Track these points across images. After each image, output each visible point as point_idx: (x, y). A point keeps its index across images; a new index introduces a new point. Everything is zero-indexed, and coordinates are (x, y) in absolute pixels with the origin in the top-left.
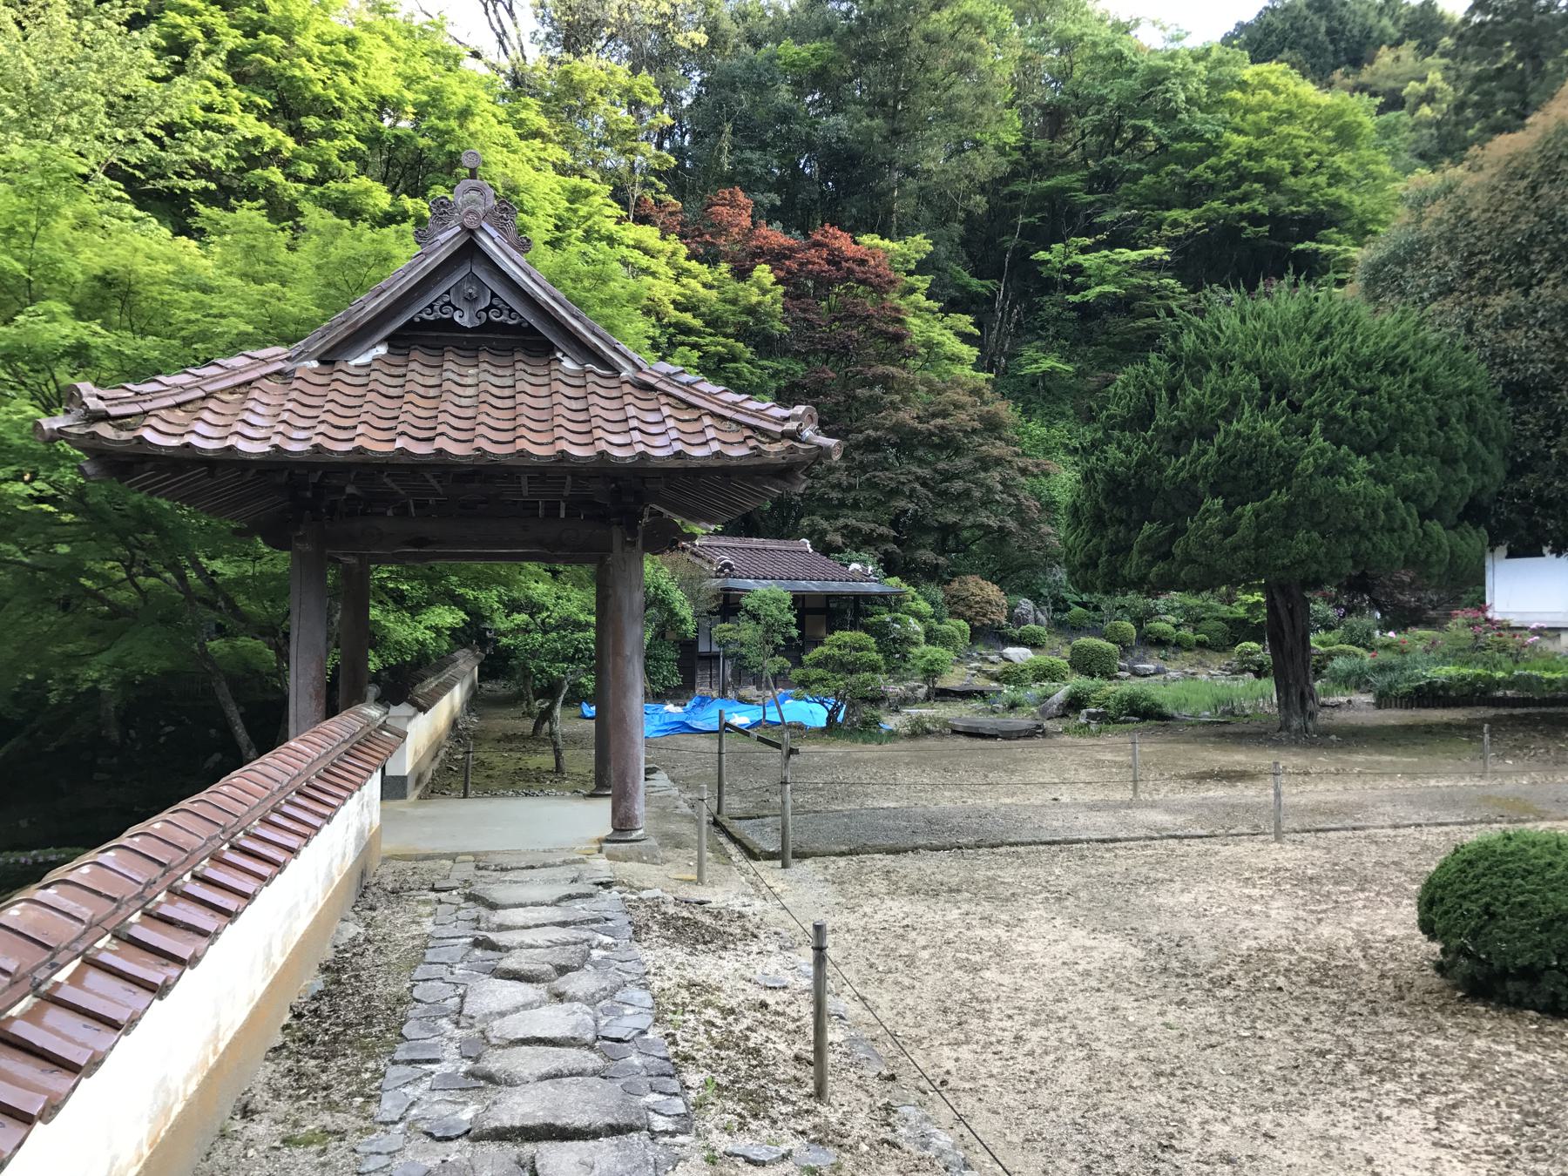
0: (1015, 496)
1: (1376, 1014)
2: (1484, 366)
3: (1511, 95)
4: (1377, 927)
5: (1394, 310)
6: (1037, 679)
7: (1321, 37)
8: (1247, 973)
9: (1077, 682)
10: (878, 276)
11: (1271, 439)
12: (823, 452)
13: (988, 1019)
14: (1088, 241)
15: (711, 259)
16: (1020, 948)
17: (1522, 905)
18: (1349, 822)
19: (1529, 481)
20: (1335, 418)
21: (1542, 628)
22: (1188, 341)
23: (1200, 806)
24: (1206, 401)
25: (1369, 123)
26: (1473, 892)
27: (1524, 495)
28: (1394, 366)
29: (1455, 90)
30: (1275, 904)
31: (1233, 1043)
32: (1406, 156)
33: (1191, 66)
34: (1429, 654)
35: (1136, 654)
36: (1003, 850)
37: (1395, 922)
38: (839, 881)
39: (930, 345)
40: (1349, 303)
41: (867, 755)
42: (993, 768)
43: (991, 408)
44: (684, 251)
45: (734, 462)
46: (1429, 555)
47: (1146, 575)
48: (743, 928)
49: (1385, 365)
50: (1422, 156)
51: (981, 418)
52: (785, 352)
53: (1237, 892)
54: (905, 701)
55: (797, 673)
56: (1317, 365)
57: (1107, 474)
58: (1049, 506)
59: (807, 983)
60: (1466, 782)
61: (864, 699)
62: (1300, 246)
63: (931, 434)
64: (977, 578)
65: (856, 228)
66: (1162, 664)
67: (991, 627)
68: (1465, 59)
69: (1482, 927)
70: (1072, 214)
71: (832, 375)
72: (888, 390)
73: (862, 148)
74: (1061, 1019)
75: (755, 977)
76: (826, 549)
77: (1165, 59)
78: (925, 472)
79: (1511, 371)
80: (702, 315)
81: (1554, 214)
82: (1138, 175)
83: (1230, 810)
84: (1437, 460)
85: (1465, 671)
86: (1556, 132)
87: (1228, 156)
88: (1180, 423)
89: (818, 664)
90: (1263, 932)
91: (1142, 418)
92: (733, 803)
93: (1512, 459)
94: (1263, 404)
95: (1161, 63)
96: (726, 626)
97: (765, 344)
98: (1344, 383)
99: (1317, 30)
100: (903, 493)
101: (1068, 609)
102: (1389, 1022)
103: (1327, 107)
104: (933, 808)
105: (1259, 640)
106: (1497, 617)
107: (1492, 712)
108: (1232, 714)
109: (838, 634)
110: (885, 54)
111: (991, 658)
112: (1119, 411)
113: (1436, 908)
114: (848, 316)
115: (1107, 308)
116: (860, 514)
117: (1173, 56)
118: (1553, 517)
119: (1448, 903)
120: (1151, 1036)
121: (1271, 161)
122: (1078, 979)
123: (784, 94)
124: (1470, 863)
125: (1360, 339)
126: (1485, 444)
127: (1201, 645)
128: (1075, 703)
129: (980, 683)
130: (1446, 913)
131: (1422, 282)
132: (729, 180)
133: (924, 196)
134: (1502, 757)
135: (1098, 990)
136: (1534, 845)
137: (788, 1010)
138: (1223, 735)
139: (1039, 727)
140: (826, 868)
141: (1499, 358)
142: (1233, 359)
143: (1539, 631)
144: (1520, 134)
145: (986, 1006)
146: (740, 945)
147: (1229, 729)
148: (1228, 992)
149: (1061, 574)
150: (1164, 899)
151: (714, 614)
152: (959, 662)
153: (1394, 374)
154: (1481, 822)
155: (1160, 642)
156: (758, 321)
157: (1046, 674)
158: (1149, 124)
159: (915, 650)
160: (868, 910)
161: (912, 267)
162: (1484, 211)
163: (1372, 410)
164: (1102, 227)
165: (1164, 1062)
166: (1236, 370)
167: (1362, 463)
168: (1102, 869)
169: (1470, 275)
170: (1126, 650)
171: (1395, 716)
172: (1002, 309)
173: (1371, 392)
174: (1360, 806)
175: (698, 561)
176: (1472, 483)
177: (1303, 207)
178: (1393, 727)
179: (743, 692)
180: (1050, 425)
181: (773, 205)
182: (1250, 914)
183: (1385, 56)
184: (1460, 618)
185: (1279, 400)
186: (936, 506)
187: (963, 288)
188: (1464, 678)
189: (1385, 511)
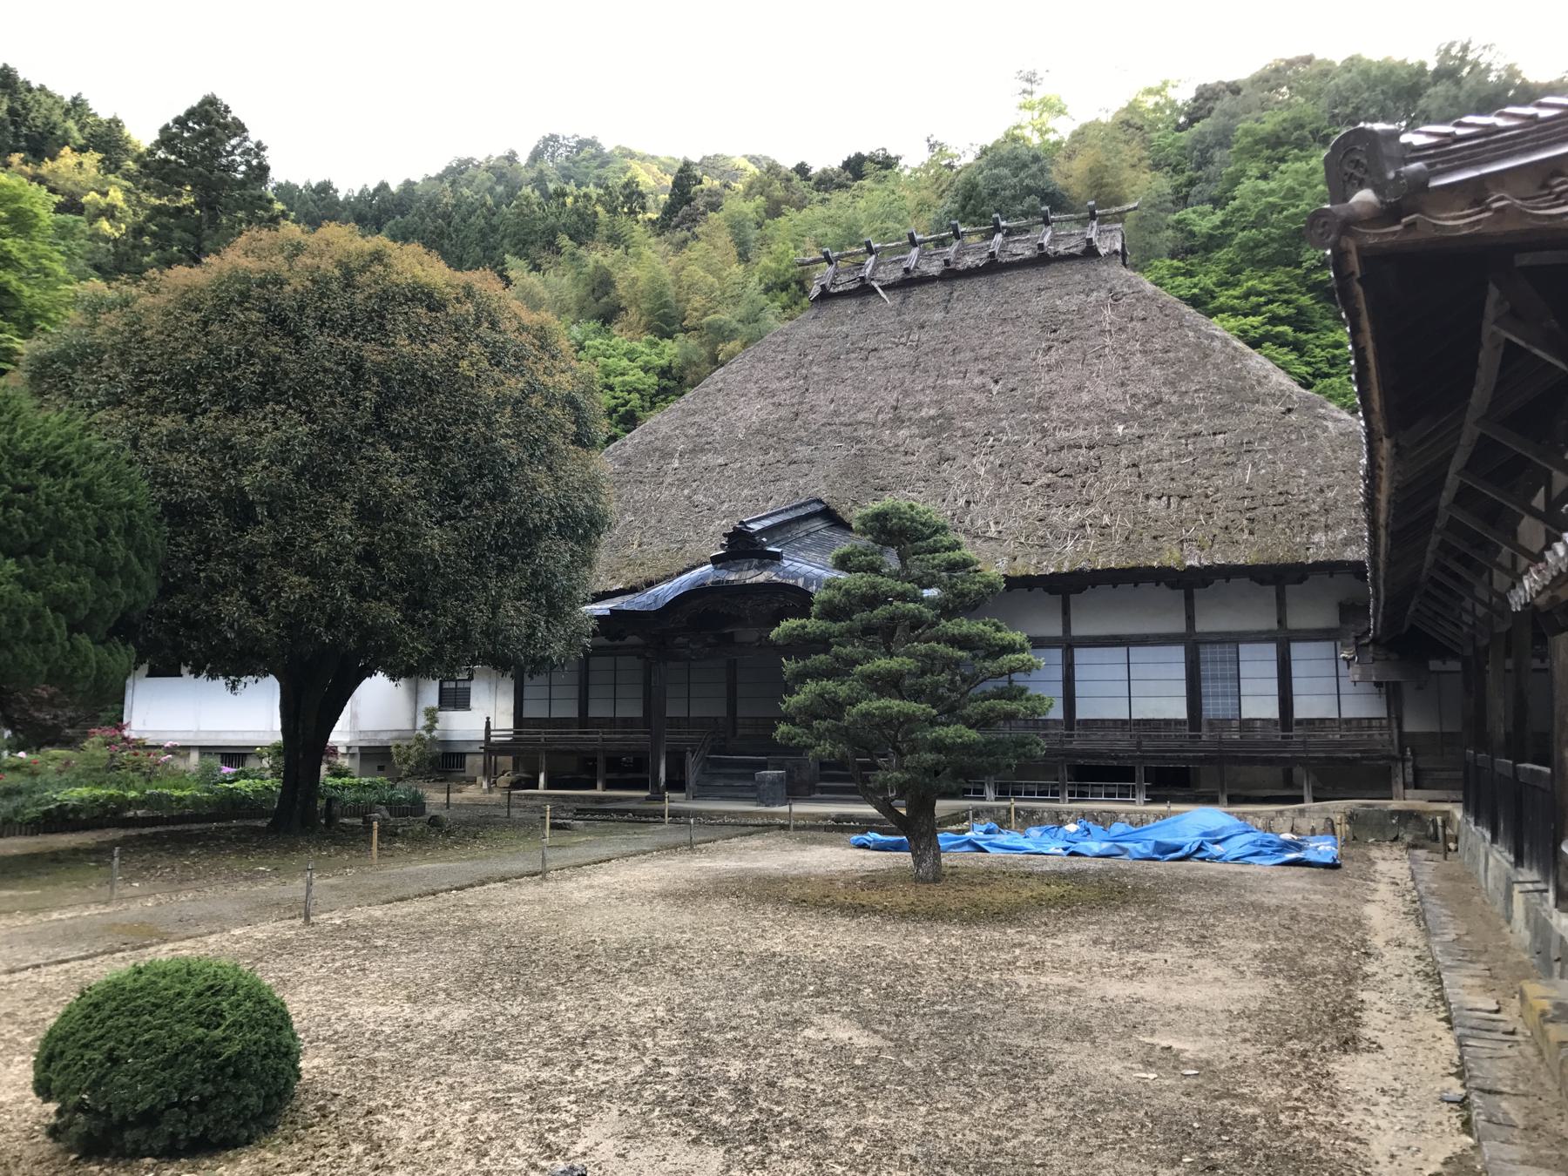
2: (146, 483)
3: (186, 236)
5: (60, 410)
17: (148, 1043)
19: (179, 601)
21: (175, 747)
25: (47, 216)
26: (96, 1039)
28: (56, 467)
29: (135, 214)
40: (10, 393)
46: (74, 670)
49: (46, 464)
50: (97, 267)
60: (93, 910)
69: (104, 1076)
79: (170, 492)
81: (221, 352)
84: (92, 571)
85: (97, 792)
86: (230, 277)
93: (165, 579)
106: (134, 736)
107: (121, 833)
118: (197, 639)
119: (69, 1055)
124: (96, 1006)
125: (20, 431)
126: (141, 561)
130: (66, 1067)
131: (91, 387)
134: (128, 880)
136: (164, 975)
141: (161, 478)
143: (173, 750)
144: (196, 270)
153: (54, 475)
154: (104, 953)
162: (158, 333)
163: (26, 511)
169: (140, 391)
173: (26, 490)
176: (124, 598)
178: (15, 857)
183: (68, 158)
184: (97, 736)
188: (96, 799)
189: (32, 620)
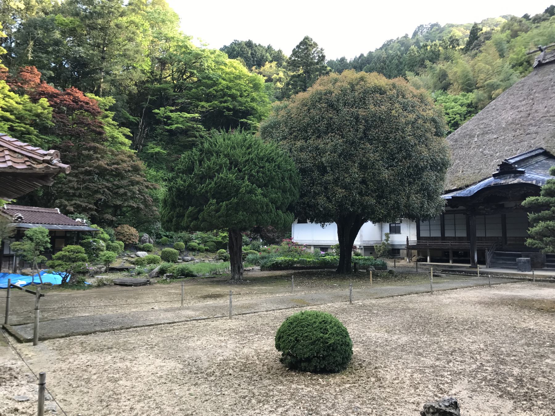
0: (144, 196)
1: (262, 380)
2: (294, 163)
3: (301, 83)
4: (262, 347)
5: (270, 143)
6: (149, 263)
7: (249, 55)
8: (219, 370)
9: (163, 264)
10: (93, 109)
11: (232, 180)
12: (62, 170)
13: (119, 402)
14: (173, 108)
15: (21, 93)
16: (135, 369)
17: (307, 336)
18: (253, 310)
20: (252, 175)
22: (206, 145)
23: (205, 307)
24: (212, 166)
26: (292, 333)
27: (304, 204)
28: (270, 160)
30: (229, 342)
31: (214, 398)
32: (273, 97)
33: (209, 54)
34: (276, 253)
35: (185, 253)
36: (131, 330)
37: (266, 346)
38: (60, 349)
39: (113, 137)
41: (78, 295)
42: (129, 297)
43: (136, 163)
44: (8, 88)
45: (19, 171)
46: (278, 221)
47: (189, 225)
48: (11, 375)
50: (277, 98)
51: (132, 166)
52: (53, 134)
53: (216, 339)
54: (96, 273)
55: (50, 262)
56: (247, 158)
57: (177, 189)
58: (156, 200)
59: (37, 397)
61: (79, 273)
62: (242, 120)
63: (112, 171)
64: (128, 226)
65: (84, 90)
66: (193, 257)
67: (132, 244)
68: (290, 70)
70: (167, 99)
71: (72, 144)
72: (95, 152)
73: (89, 61)
74: (150, 398)
75: (14, 397)
76: (66, 212)
77: (201, 51)
78: (109, 185)
80: (15, 114)
82: (191, 89)
83: (215, 308)
84: (281, 191)
85: (286, 258)
87: (220, 87)
88: (203, 173)
89: (59, 259)
90: (225, 353)
91: (189, 170)
92: (13, 319)
94: (230, 169)
95: (200, 52)
96: (17, 243)
97: (44, 130)
98: (255, 164)
99: (248, 53)
100: (100, 192)
101: (161, 237)
102: (266, 382)
103: (251, 77)
104: (104, 314)
105: (225, 249)
106: (295, 242)
107: (293, 271)
108: (216, 274)
109: (68, 246)
110: (100, 28)
111: (132, 256)
112: (182, 167)
113: (281, 340)
114: (81, 123)
115: (179, 132)
116: (82, 199)
117: (204, 51)
118: (311, 211)
120: (184, 400)
121: (234, 91)
122: (157, 380)
123: (57, 35)
124: (291, 323)
127: (207, 250)
128: (162, 272)
129: (127, 265)
130: (284, 341)
131: (278, 135)
132: (32, 63)
133: (113, 82)
135: (165, 383)
137: (28, 411)
138: (212, 282)
139: (148, 281)
140: (54, 344)
141: (299, 161)
142: (221, 153)
145: (119, 396)
146: (8, 383)
147: (215, 279)
148: (213, 378)
149: (159, 225)
150: (191, 344)
151: (12, 238)
152: (119, 257)
153: (269, 162)
155: (193, 249)
156: (41, 120)
157: (152, 261)
158: (195, 72)
159: (101, 253)
160: (71, 360)
161: (107, 108)
164: (177, 104)
165: (189, 410)
166: (222, 156)
167: (260, 191)
168: (169, 334)
169: (291, 134)
170: (181, 252)
171: (266, 273)
172: (141, 128)
173: (263, 167)
174: (256, 305)
175: (6, 215)
177: (243, 108)
178: (266, 277)
179: (24, 271)
180: (157, 171)
181: (51, 76)
182: (221, 347)
183: (267, 65)
185: (235, 168)
186: (113, 198)
187: (127, 119)
189: (266, 206)
